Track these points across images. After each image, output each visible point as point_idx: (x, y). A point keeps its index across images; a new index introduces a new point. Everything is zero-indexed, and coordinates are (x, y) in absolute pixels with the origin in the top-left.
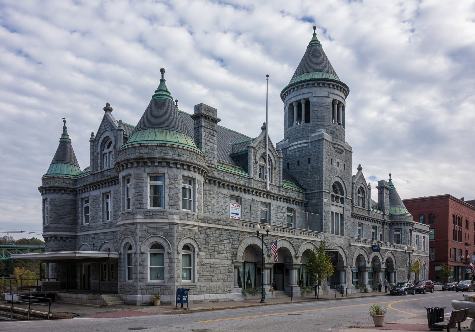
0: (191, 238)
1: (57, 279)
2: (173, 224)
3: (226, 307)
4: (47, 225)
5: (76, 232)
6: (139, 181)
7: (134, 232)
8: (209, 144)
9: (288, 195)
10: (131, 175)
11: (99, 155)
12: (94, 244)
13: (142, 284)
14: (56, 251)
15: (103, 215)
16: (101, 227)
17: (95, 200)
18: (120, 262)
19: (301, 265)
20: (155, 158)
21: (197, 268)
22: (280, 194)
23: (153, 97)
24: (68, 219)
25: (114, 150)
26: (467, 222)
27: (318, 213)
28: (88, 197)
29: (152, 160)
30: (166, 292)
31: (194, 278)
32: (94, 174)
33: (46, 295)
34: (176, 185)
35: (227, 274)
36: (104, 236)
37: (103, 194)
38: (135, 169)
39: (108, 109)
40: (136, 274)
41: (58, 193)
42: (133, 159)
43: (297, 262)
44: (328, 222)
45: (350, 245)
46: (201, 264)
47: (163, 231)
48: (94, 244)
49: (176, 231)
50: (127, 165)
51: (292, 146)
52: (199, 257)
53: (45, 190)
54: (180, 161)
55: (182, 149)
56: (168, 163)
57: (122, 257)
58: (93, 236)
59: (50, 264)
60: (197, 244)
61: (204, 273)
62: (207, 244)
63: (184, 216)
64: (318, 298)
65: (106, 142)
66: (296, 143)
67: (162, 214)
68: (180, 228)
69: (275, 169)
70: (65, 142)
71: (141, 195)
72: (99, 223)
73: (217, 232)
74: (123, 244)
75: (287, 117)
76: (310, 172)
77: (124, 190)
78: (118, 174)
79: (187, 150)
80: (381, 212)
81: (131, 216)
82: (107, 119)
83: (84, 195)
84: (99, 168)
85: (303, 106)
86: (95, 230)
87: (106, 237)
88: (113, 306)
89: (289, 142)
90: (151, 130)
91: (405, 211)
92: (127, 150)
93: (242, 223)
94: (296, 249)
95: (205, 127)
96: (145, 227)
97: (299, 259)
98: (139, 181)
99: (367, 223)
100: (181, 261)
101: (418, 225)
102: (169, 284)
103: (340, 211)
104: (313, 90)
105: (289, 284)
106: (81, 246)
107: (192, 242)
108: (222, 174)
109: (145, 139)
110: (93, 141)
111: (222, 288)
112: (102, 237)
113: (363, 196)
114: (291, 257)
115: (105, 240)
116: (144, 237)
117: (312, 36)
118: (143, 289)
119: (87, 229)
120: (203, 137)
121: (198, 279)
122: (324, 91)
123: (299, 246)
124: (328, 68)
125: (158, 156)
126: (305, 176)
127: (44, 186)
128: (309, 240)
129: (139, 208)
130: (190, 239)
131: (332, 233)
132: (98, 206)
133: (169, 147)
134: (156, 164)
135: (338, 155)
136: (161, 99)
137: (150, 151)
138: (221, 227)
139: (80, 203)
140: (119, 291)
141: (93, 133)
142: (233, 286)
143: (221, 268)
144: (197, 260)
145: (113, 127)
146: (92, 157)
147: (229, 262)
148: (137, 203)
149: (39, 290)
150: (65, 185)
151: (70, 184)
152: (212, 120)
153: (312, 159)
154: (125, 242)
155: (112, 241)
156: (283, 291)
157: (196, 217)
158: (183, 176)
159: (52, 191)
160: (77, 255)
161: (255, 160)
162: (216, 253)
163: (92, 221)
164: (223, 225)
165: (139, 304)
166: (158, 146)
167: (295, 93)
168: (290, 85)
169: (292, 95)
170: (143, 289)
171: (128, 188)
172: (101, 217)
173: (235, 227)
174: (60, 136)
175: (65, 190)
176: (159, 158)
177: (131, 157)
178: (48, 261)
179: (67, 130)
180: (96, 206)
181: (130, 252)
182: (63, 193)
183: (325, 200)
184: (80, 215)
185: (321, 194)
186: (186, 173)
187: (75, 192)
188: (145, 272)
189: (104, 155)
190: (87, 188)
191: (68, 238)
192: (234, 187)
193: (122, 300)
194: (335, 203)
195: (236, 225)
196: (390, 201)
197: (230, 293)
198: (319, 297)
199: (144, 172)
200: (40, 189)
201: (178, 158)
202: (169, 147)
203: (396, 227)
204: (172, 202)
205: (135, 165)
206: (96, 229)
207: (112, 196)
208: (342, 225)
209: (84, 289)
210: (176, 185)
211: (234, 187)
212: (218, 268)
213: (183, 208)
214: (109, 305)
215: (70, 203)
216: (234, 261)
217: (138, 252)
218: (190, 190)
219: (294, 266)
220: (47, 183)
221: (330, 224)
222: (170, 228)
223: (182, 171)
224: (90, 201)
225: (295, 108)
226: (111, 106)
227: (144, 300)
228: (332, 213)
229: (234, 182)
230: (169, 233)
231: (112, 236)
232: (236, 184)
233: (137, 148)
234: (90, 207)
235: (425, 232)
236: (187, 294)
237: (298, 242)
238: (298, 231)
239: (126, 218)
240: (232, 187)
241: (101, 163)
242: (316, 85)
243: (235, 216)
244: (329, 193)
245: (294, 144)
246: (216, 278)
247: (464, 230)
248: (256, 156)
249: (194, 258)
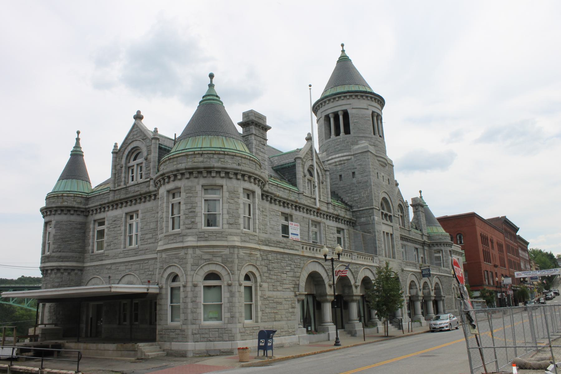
0: (253, 265)
1: (56, 325)
2: (234, 247)
3: (303, 354)
4: (47, 253)
5: (83, 262)
6: (190, 195)
7: (183, 259)
8: (261, 154)
9: (335, 213)
10: (180, 188)
11: (123, 168)
12: (110, 277)
13: (194, 326)
14: (57, 287)
15: (125, 239)
16: (121, 255)
17: (114, 221)
18: (161, 299)
19: (306, 295)
20: (214, 168)
21: (259, 303)
22: (328, 211)
23: (200, 103)
24: (76, 246)
25: (144, 162)
26: (492, 242)
27: (370, 232)
28: (104, 218)
29: (209, 171)
30: (226, 337)
31: (257, 317)
32: (115, 191)
33: (50, 346)
35: (291, 310)
36: (126, 265)
37: (127, 214)
38: (186, 181)
39: (138, 117)
41: (66, 214)
42: (186, 169)
43: (357, 292)
44: (382, 244)
45: (403, 270)
46: (265, 299)
47: (221, 256)
48: (110, 277)
49: (238, 256)
50: (175, 176)
51: (332, 159)
52: (262, 289)
53: (51, 211)
54: (241, 170)
55: (242, 157)
56: (227, 173)
57: (164, 291)
58: (109, 267)
59: (48, 305)
60: (259, 271)
61: (268, 310)
62: (269, 272)
63: (245, 237)
64: (388, 336)
65: (133, 153)
66: (337, 156)
67: (220, 235)
68: (242, 252)
69: (323, 183)
70: (77, 156)
71: (194, 212)
72: (119, 250)
73: (279, 256)
74: (166, 275)
75: (323, 129)
76: (356, 186)
77: (168, 207)
79: (247, 159)
80: (419, 232)
81: (180, 239)
82: (137, 127)
83: (99, 216)
84: (122, 184)
85: (332, 120)
86: (111, 259)
87: (129, 267)
88: (154, 359)
89: (328, 155)
90: (204, 136)
91: (441, 230)
92: (175, 159)
93: (302, 246)
94: (354, 275)
95: (255, 135)
96: (198, 252)
97: (359, 288)
98: (190, 195)
99: (409, 244)
100: (243, 295)
102: (230, 326)
103: (388, 230)
104: (351, 101)
105: (349, 320)
106: (91, 279)
107: (254, 270)
108: (273, 188)
109: (199, 146)
110: (117, 153)
111: (286, 329)
112: (122, 268)
113: (402, 214)
114: (351, 286)
115: (127, 271)
116: (197, 265)
117: (208, 88)
118: (196, 334)
119: (100, 257)
120: (254, 146)
121: (261, 319)
122: (363, 103)
123: (357, 272)
124: (360, 80)
125: (216, 165)
126: (350, 191)
127: (50, 206)
128: (366, 265)
129: (190, 228)
130: (251, 266)
131: (386, 256)
132: (118, 229)
133: (228, 154)
134: (213, 174)
135: (382, 168)
136: (212, 104)
137: (205, 160)
138: (282, 250)
139: (92, 226)
140: (158, 337)
141: (116, 144)
142: (297, 326)
143: (284, 302)
144: (259, 293)
145: (145, 135)
146: (114, 170)
147: (292, 294)
148: (188, 221)
149: (36, 340)
150: (75, 205)
151: (81, 203)
152: (263, 128)
153: (356, 173)
154: (169, 271)
155: (137, 272)
156: (343, 330)
157: (257, 238)
158: (244, 189)
159: (59, 212)
160: (113, 290)
161: (304, 172)
162: (278, 284)
163: (109, 248)
164: (284, 248)
165: (190, 355)
166: (215, 154)
167: (331, 105)
168: (322, 99)
169: (327, 106)
170: (196, 334)
171: (173, 205)
172: (123, 242)
173: (296, 250)
174: (72, 149)
175: (75, 211)
176: (218, 168)
177: (182, 166)
178: (44, 300)
179: (81, 141)
180: (116, 229)
181: (175, 284)
182: (72, 214)
183: (376, 218)
184: (91, 241)
185: (371, 211)
186: (247, 185)
187: (86, 212)
188: (198, 311)
189: (129, 168)
190: (103, 208)
191: (73, 270)
192: (285, 203)
193: (164, 351)
194: (385, 221)
195: (297, 247)
196: (426, 220)
197: (294, 335)
198: (389, 334)
199: (198, 184)
200: (42, 210)
201: (239, 168)
202: (228, 154)
203: (436, 248)
204: (231, 221)
205: (187, 175)
206: (115, 257)
207: (140, 216)
208: (393, 247)
209: (91, 336)
210: (236, 200)
211: (285, 203)
212: (281, 303)
214: (150, 357)
215: (79, 226)
216: (297, 293)
217: (190, 284)
218: (249, 205)
219: (354, 298)
220: (54, 202)
221: (383, 246)
222: (230, 253)
223: (242, 182)
224: (106, 223)
225: (332, 120)
226: (142, 114)
227: (197, 349)
228: (384, 232)
229: (285, 197)
230: (229, 259)
231: (138, 266)
232: (287, 200)
233: (190, 157)
234: (106, 231)
236: (272, 338)
237: (357, 268)
238: (355, 254)
239: (172, 241)
240: (284, 203)
241: (125, 178)
242: (354, 97)
243: (295, 237)
244: (379, 210)
245: (334, 156)
246: (280, 316)
247: (491, 251)
248: (303, 168)
249: (256, 290)
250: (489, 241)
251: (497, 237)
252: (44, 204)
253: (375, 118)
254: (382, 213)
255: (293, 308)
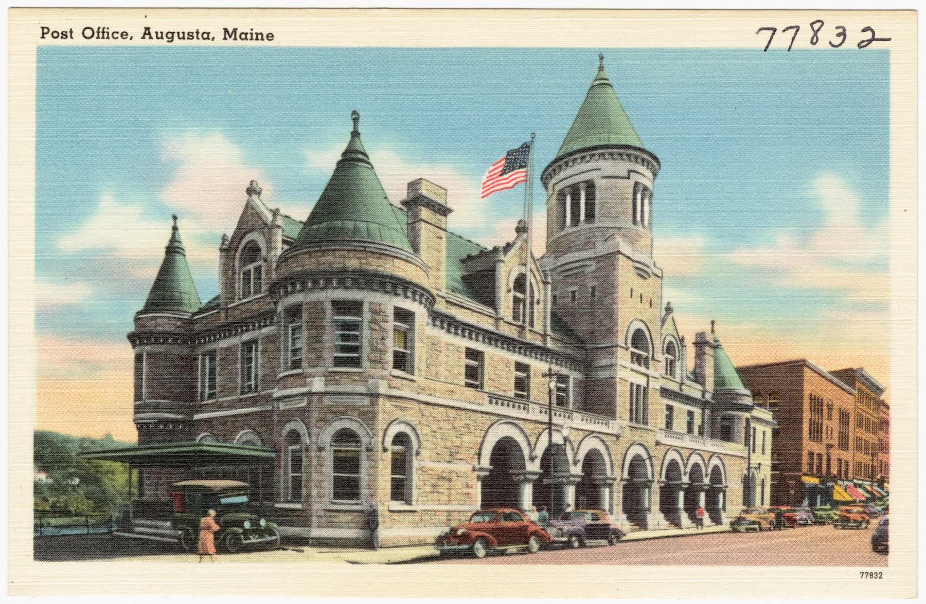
26: (830, 408)
34: (382, 324)
35: (465, 490)
40: (308, 487)
78: (276, 303)
80: (699, 387)
101: (758, 413)
103: (642, 381)
104: (602, 163)
110: (228, 249)
210: (382, 324)
213: (395, 367)
217: (314, 447)
235: (767, 423)
247: (826, 422)
250: (825, 408)
251: (844, 400)
252: (131, 328)
253: (639, 196)
254: (633, 353)
255: (468, 486)
